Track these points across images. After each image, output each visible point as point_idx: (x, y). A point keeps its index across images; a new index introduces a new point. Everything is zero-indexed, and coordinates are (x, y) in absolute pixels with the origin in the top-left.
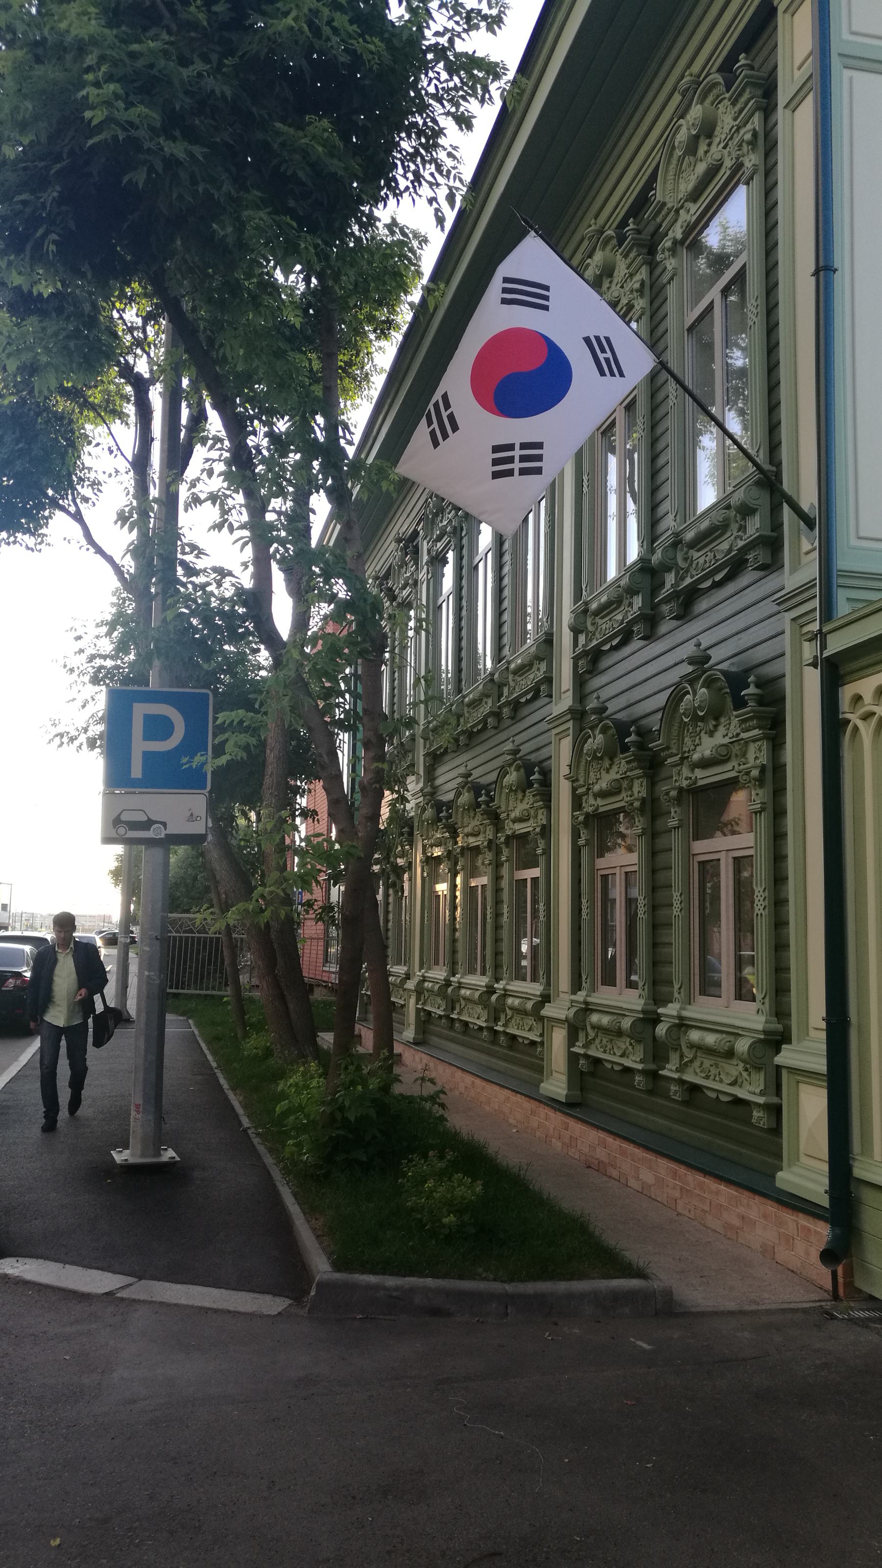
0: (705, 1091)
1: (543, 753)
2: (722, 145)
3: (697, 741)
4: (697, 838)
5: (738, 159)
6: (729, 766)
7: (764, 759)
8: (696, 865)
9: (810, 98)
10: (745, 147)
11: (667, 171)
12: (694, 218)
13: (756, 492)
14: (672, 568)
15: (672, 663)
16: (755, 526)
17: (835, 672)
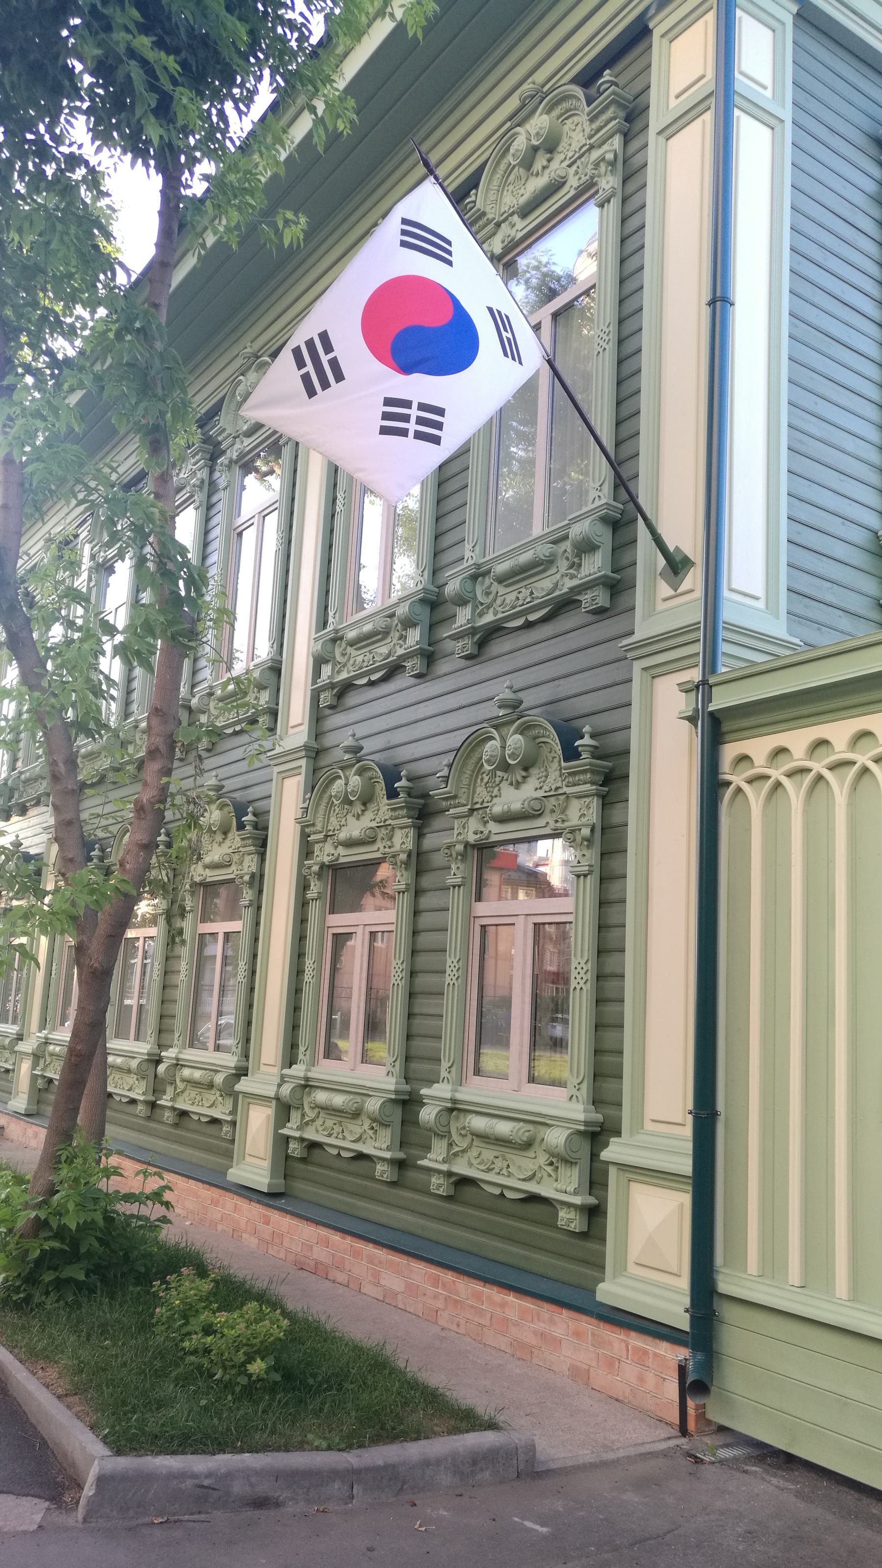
0: (483, 1186)
1: (256, 792)
2: (567, 163)
3: (496, 792)
4: (332, 911)
5: (592, 178)
6: (541, 822)
7: (410, 845)
8: (330, 937)
9: (708, 116)
10: (603, 167)
11: (494, 171)
12: (520, 235)
13: (418, 608)
14: (469, 601)
15: (456, 706)
16: (595, 565)
17: (715, 729)
